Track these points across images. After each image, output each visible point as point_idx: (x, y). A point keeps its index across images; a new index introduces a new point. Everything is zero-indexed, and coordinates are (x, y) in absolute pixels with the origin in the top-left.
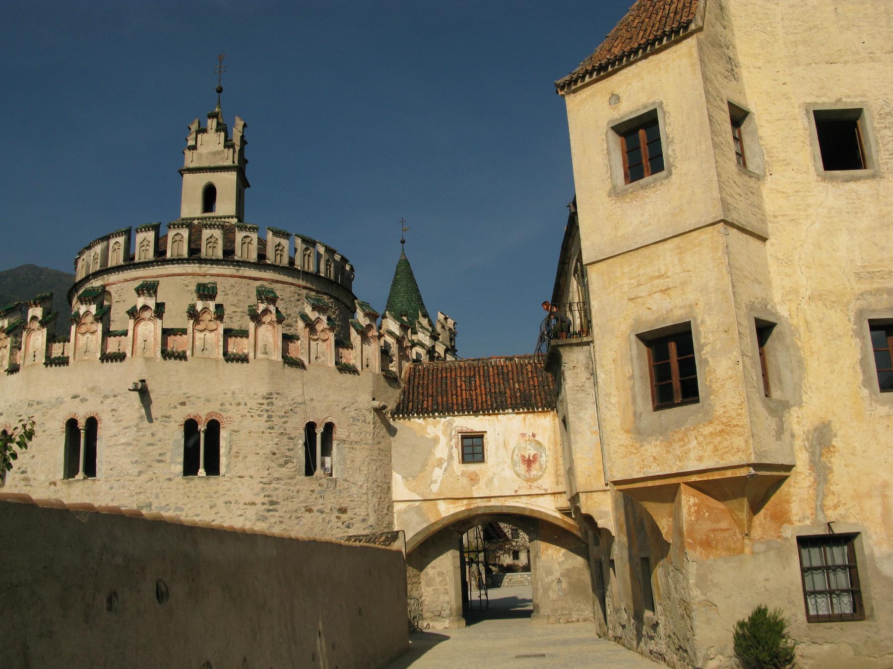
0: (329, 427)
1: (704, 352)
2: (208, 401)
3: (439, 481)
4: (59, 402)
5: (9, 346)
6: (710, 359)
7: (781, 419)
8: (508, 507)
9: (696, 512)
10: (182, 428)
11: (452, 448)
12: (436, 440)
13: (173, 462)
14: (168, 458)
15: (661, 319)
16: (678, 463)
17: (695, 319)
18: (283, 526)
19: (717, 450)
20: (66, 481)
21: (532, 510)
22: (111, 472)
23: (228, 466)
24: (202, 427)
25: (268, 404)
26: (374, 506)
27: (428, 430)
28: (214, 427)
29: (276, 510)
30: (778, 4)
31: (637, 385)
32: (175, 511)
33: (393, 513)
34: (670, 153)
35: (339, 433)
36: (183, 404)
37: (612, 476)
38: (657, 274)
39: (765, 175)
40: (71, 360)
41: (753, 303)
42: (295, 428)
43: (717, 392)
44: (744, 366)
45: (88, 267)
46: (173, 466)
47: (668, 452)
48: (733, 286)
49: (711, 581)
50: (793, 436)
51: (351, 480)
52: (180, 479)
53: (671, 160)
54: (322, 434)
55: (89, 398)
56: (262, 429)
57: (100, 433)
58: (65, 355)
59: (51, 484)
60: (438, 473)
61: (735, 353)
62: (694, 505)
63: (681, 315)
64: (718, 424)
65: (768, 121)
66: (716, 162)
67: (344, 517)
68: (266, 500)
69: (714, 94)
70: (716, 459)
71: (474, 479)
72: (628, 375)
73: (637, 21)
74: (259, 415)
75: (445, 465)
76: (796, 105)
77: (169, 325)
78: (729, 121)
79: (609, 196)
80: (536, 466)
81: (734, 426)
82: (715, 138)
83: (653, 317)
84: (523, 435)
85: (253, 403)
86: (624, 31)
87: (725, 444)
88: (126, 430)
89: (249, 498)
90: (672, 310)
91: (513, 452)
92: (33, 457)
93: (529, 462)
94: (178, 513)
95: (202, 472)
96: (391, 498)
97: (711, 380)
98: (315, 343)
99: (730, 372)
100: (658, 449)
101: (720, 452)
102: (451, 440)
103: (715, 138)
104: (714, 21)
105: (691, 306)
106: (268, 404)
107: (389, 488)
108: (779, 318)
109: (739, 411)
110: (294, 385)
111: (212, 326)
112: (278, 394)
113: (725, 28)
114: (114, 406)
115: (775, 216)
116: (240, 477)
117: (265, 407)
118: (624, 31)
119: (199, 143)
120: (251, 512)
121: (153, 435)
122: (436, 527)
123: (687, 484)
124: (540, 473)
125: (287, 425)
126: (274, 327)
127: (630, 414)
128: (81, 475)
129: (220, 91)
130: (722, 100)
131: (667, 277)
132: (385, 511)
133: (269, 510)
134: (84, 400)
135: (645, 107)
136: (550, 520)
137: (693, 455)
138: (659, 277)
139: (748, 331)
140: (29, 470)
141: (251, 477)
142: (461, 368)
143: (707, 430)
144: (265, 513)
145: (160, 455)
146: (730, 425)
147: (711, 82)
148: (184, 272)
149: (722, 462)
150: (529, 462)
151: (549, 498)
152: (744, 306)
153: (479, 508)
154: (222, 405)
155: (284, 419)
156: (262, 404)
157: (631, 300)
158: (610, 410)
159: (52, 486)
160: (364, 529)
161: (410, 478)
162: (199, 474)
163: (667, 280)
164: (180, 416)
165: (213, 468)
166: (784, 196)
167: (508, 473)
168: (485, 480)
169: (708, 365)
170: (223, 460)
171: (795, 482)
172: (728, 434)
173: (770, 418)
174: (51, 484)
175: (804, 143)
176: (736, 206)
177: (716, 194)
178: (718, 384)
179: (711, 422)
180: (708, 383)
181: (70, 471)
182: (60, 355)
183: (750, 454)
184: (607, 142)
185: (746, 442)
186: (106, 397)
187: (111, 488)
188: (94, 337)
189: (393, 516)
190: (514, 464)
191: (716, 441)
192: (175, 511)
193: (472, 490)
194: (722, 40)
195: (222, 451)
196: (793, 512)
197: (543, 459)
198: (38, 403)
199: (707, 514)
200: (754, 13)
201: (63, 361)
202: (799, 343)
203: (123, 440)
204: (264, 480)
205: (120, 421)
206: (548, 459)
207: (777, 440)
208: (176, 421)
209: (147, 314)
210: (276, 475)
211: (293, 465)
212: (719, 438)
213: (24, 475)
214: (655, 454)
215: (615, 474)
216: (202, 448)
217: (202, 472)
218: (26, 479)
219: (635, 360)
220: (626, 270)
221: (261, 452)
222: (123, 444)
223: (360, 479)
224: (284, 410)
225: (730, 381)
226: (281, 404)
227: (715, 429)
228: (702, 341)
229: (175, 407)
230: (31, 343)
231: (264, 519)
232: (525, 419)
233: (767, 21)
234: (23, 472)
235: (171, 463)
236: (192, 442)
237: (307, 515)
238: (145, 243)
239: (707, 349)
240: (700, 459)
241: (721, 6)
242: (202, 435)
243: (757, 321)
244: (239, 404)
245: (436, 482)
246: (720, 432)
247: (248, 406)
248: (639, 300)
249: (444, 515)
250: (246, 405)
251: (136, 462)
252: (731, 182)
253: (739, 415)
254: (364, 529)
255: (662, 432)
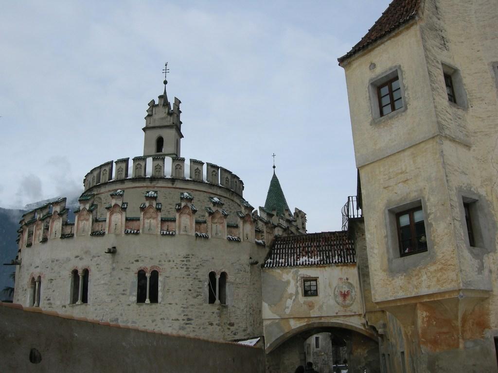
0: (224, 275)
1: (430, 218)
2: (152, 259)
3: (290, 307)
4: (68, 260)
5: (43, 228)
6: (433, 223)
7: (481, 261)
8: (332, 323)
9: (427, 321)
10: (137, 275)
11: (298, 287)
12: (288, 282)
13: (131, 294)
14: (128, 292)
15: (403, 199)
16: (415, 290)
17: (423, 198)
18: (195, 334)
19: (440, 281)
20: (71, 305)
21: (352, 326)
22: (96, 300)
23: (162, 298)
24: (148, 275)
25: (187, 261)
26: (251, 322)
27: (284, 277)
28: (155, 275)
29: (191, 324)
30: (472, 4)
31: (390, 241)
32: (132, 323)
33: (263, 326)
34: (406, 96)
35: (230, 278)
36: (137, 261)
37: (375, 299)
38: (400, 171)
39: (468, 107)
40: (75, 236)
41: (461, 186)
42: (203, 275)
43: (438, 244)
44: (455, 227)
45: (90, 184)
46: (131, 297)
47: (409, 283)
48: (447, 176)
49: (438, 366)
50: (490, 271)
51: (237, 306)
52: (135, 306)
53: (407, 100)
54: (220, 279)
55: (84, 257)
56: (183, 276)
57: (90, 278)
58: (72, 233)
59: (63, 306)
60: (289, 302)
61: (449, 218)
62: (426, 316)
63: (415, 196)
64: (439, 264)
65: (469, 74)
66: (434, 99)
67: (232, 328)
68: (185, 318)
69: (432, 58)
70: (439, 287)
71: (311, 306)
72: (384, 235)
73: (386, 19)
74: (181, 268)
75: (294, 297)
76: (486, 64)
77: (130, 216)
78: (443, 74)
79: (371, 125)
80: (349, 298)
81: (449, 265)
82: (433, 85)
83: (398, 198)
84: (341, 279)
85: (178, 261)
86: (378, 26)
87: (444, 277)
88: (105, 276)
89: (175, 316)
90: (409, 193)
91: (335, 289)
92: (54, 291)
93: (345, 296)
94: (133, 324)
95: (148, 301)
96: (262, 317)
97: (434, 237)
98: (215, 225)
99: (446, 231)
100: (403, 281)
101: (441, 282)
102: (297, 282)
103: (433, 85)
104: (431, 15)
105: (421, 190)
106: (187, 261)
107: (260, 311)
108: (480, 196)
109: (452, 255)
110: (203, 251)
111: (154, 215)
112: (193, 255)
113: (439, 19)
114: (98, 262)
115: (475, 133)
116: (170, 304)
117: (185, 263)
118: (378, 26)
119: (154, 113)
120: (176, 325)
121: (120, 279)
122: (289, 335)
123: (421, 303)
124: (352, 302)
125: (198, 274)
126: (191, 216)
127: (386, 260)
128: (79, 302)
129: (165, 82)
130: (438, 62)
131: (407, 173)
132: (258, 325)
133: (187, 324)
134: (81, 259)
135: (391, 69)
136: (358, 330)
137: (423, 285)
138: (401, 173)
139: (457, 204)
140: (51, 299)
141: (176, 304)
142: (303, 239)
143: (432, 268)
144: (185, 326)
145: (124, 290)
146: (446, 265)
147: (430, 51)
148: (142, 185)
149: (442, 288)
150: (345, 296)
151: (356, 318)
152: (454, 188)
153: (314, 323)
154: (160, 261)
155: (196, 270)
156: (183, 261)
157: (385, 188)
158: (373, 258)
159: (64, 308)
160: (245, 336)
161: (273, 306)
162: (146, 302)
163: (406, 174)
164: (135, 268)
165: (154, 299)
166: (481, 119)
167: (332, 302)
168: (318, 307)
169: (432, 226)
170: (160, 294)
171: (492, 301)
172: (445, 270)
173: (473, 259)
174: (63, 306)
175: (492, 86)
176: (448, 126)
177: (434, 119)
178: (438, 239)
179: (435, 263)
180: (433, 238)
181: (74, 300)
182: (69, 233)
183: (460, 283)
184: (369, 93)
185: (457, 275)
186: (94, 257)
187: (96, 310)
188: (88, 222)
189: (263, 329)
190: (336, 296)
191: (438, 276)
192: (132, 323)
193: (310, 313)
194: (438, 26)
195: (159, 288)
196: (491, 321)
197: (353, 294)
198: (57, 261)
199: (435, 323)
200: (457, 10)
201: (71, 236)
202: (493, 212)
203: (102, 282)
204: (184, 306)
205: (102, 271)
206: (356, 293)
207: (479, 274)
208: (133, 271)
209: (118, 209)
210: (191, 303)
211: (201, 297)
212: (440, 274)
213: (49, 301)
214: (401, 285)
215: (377, 297)
216: (148, 288)
217: (148, 301)
218: (50, 304)
219: (388, 225)
220: (382, 169)
221: (182, 289)
222: (103, 284)
223: (242, 306)
224: (196, 265)
225: (446, 236)
226: (194, 261)
227: (438, 268)
228: (429, 212)
229: (133, 263)
230: (54, 226)
231: (183, 328)
232: (342, 269)
233: (466, 14)
234: (49, 300)
235: (130, 295)
236: (143, 281)
237: (210, 327)
238: (120, 170)
239: (432, 216)
240: (429, 287)
241: (436, 6)
242: (148, 279)
243: (464, 198)
244: (170, 261)
245: (288, 308)
246: (441, 269)
247: (175, 262)
248: (390, 188)
249: (293, 327)
250: (174, 261)
251: (110, 295)
252: (445, 112)
253: (452, 258)
254: (245, 336)
255: (405, 270)
